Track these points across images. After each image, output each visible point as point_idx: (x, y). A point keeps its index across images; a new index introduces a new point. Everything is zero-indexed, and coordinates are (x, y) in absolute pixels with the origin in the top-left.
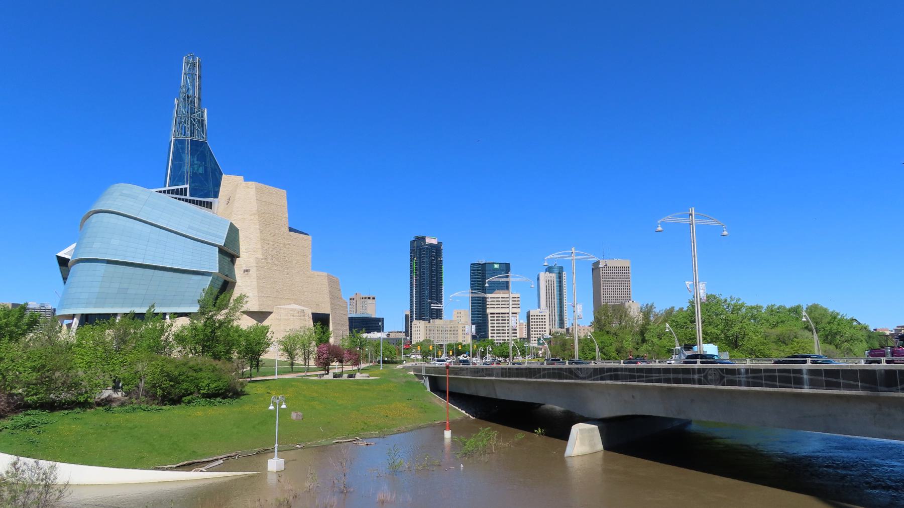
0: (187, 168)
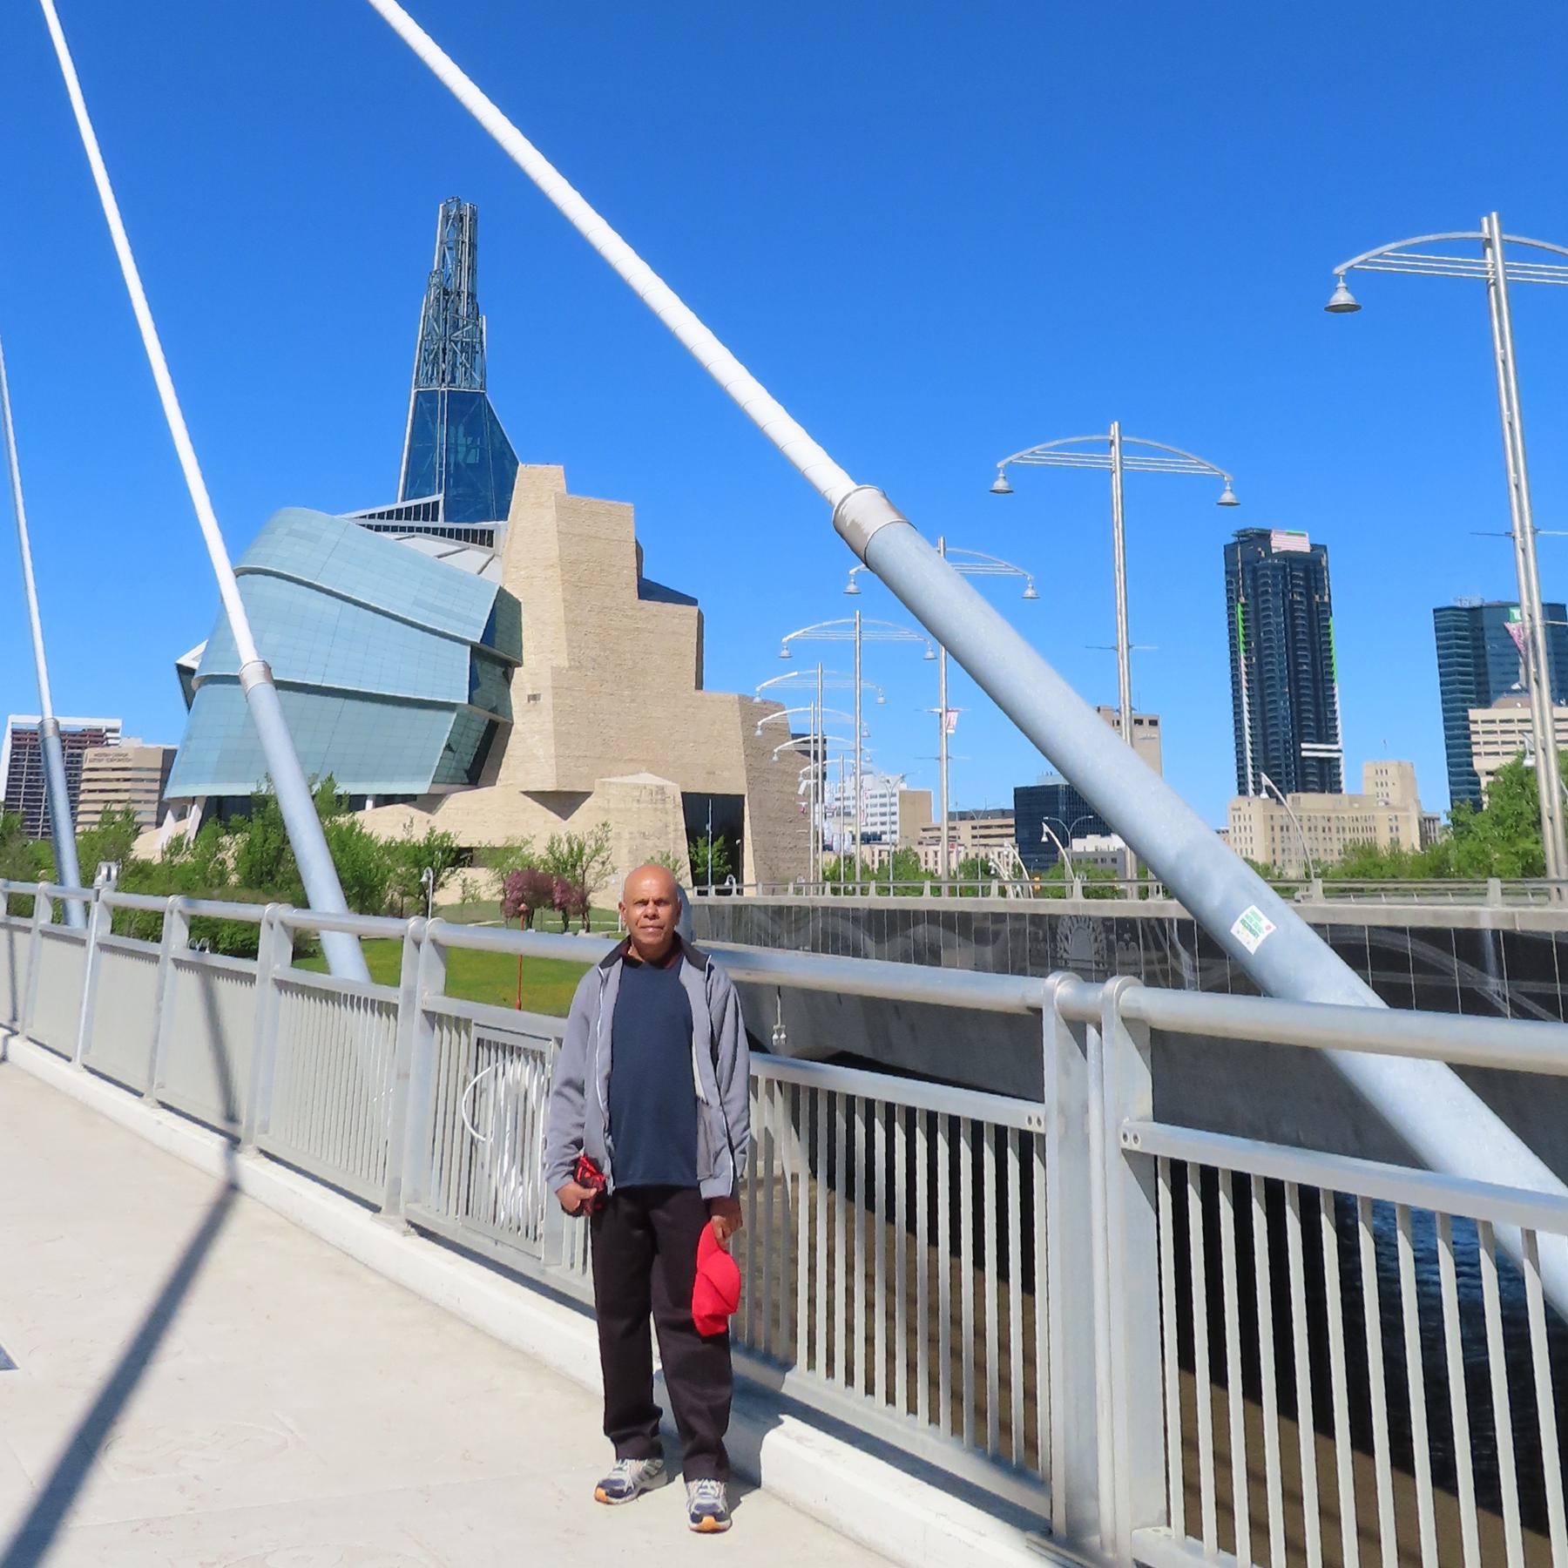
0: (439, 457)
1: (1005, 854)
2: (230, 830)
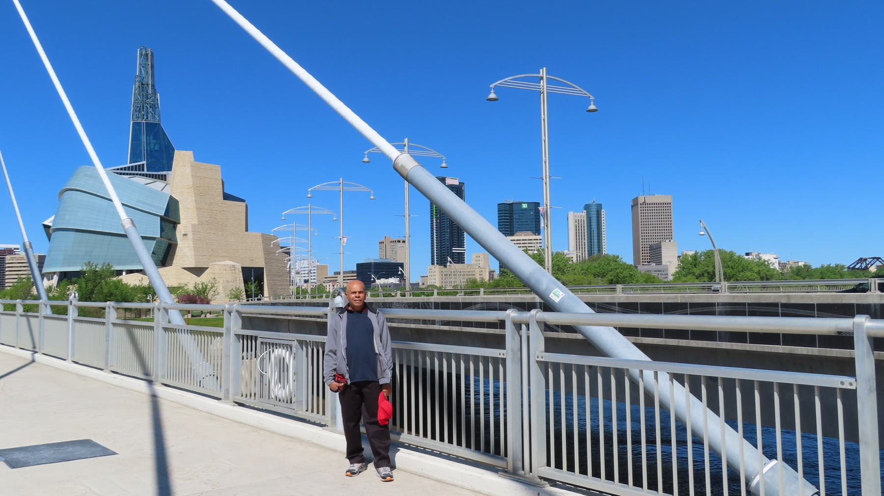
0: (144, 146)
1: (357, 286)
2: (72, 283)
